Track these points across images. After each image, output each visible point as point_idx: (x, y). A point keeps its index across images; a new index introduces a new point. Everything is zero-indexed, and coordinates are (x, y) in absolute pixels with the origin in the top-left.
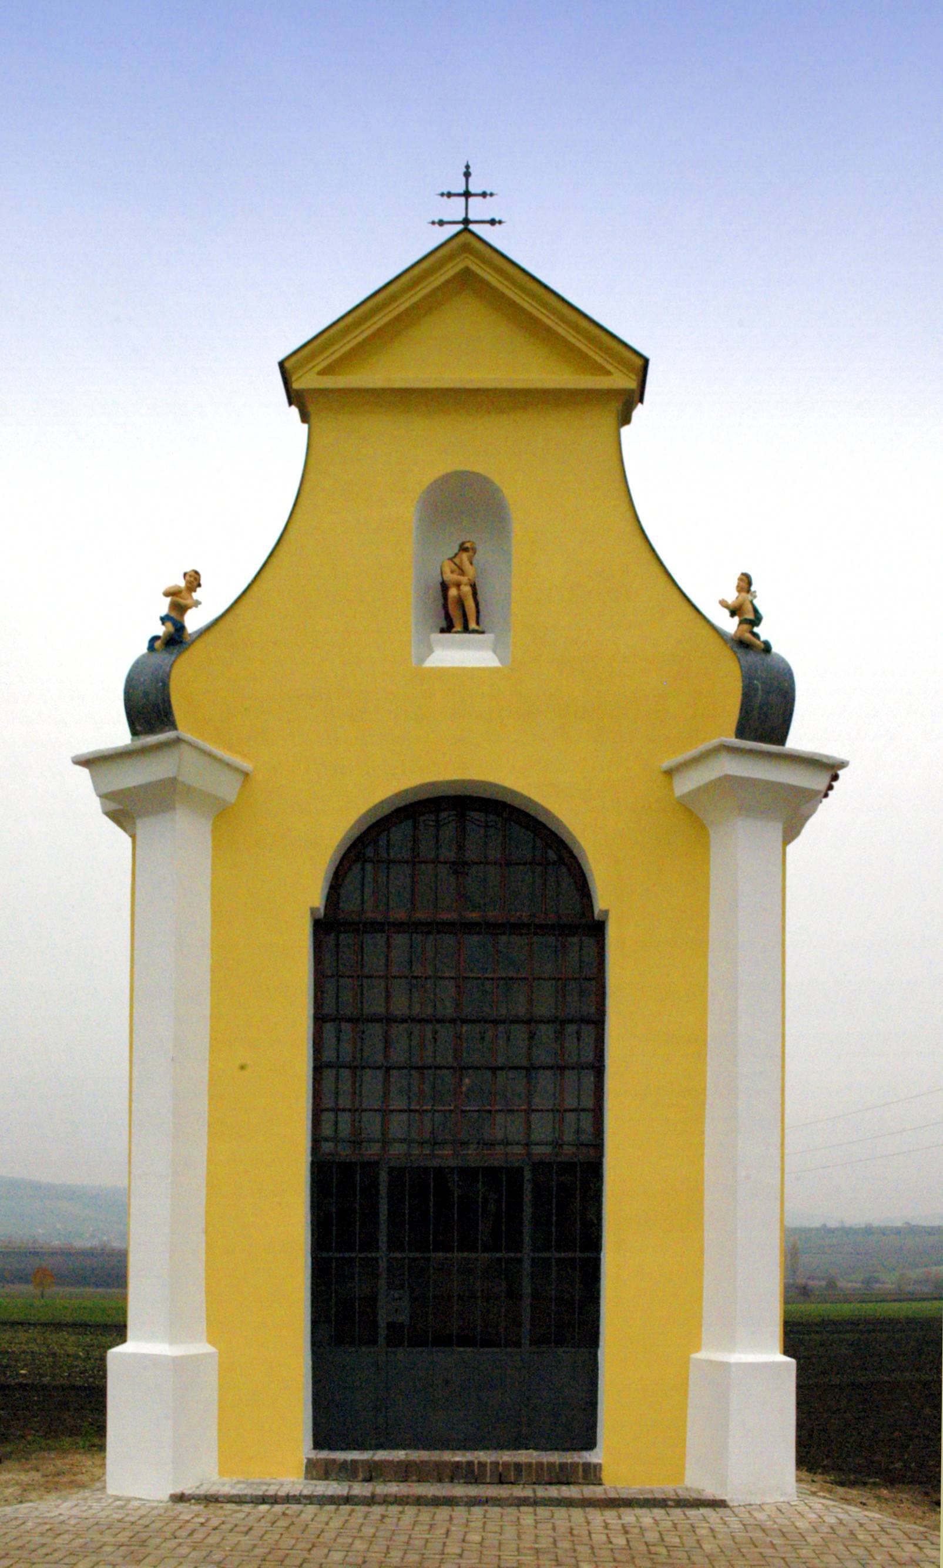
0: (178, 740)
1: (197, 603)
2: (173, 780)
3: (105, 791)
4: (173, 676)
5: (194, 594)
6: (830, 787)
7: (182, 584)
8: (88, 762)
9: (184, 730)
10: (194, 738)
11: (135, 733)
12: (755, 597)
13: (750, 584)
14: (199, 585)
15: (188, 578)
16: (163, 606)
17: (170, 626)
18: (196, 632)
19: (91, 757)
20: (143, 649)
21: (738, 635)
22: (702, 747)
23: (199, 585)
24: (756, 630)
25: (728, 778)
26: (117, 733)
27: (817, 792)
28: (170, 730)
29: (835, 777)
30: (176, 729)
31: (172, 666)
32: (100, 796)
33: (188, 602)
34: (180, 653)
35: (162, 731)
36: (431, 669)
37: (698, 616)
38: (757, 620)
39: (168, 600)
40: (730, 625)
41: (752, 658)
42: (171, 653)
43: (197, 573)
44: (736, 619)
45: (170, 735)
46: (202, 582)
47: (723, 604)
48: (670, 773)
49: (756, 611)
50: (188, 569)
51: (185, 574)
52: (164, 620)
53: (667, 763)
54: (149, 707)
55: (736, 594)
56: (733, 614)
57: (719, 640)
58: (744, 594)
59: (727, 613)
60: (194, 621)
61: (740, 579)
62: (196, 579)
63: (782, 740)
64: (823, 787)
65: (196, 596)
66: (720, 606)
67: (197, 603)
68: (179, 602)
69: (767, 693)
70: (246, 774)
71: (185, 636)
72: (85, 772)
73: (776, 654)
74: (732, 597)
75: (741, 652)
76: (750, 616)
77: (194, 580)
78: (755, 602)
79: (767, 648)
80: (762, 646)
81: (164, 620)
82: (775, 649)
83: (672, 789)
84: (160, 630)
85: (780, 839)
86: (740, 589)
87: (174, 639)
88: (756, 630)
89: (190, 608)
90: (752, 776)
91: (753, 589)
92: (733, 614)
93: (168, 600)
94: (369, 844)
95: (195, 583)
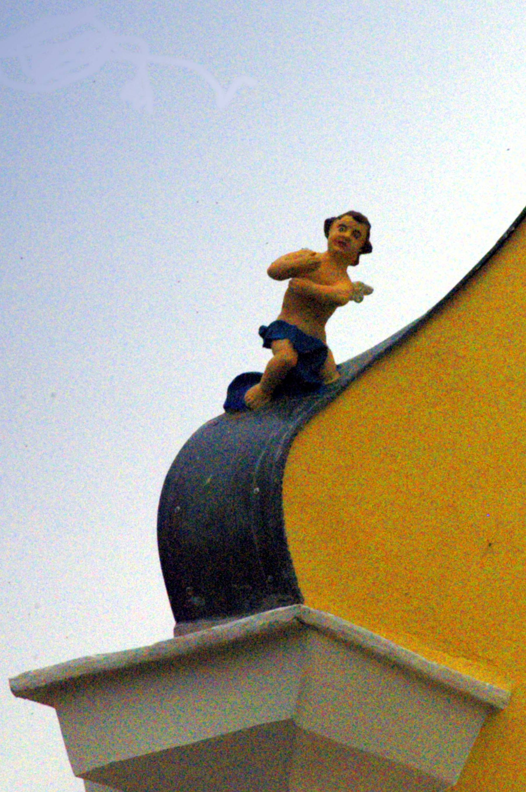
0: (302, 628)
1: (360, 292)
2: (290, 723)
3: (88, 768)
4: (293, 469)
5: (351, 270)
7: (320, 245)
8: (63, 690)
9: (319, 603)
10: (347, 623)
11: (183, 612)
14: (367, 248)
15: (334, 232)
16: (271, 301)
17: (285, 349)
18: (355, 360)
19: (61, 676)
20: (215, 407)
23: (367, 248)
26: (140, 615)
28: (283, 603)
30: (296, 597)
31: (288, 445)
32: (85, 776)
33: (339, 287)
34: (312, 414)
35: (254, 608)
39: (284, 285)
42: (288, 417)
43: (359, 218)
45: (281, 614)
46: (373, 240)
50: (336, 211)
51: (328, 224)
52: (268, 335)
54: (223, 543)
60: (348, 336)
62: (356, 234)
65: (355, 274)
67: (360, 292)
68: (312, 290)
70: (491, 710)
71: (327, 370)
72: (48, 714)
77: (352, 237)
81: (268, 335)
84: (259, 359)
87: (298, 378)
89: (341, 303)
93: (284, 285)
94: (386, 700)
95: (355, 244)
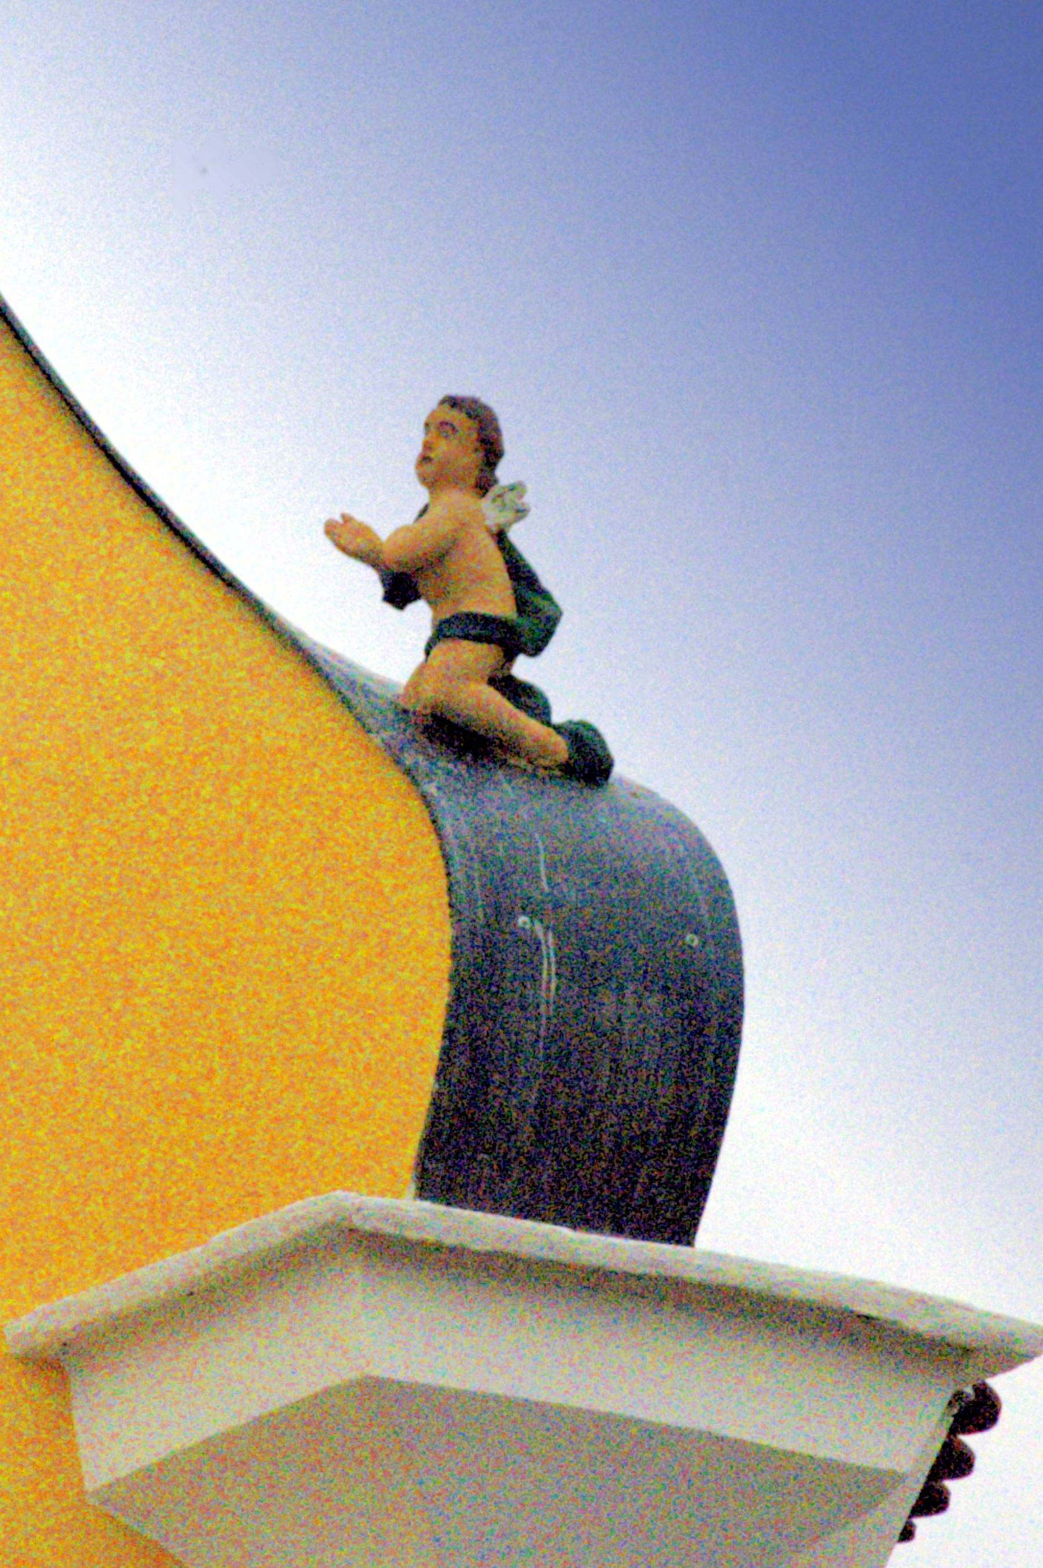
6: (954, 1462)
12: (521, 513)
13: (491, 451)
21: (429, 693)
22: (234, 1238)
24: (523, 668)
25: (382, 1400)
27: (881, 1483)
29: (978, 1411)
36: (960, 1443)
37: (217, 591)
38: (525, 622)
40: (390, 647)
41: (514, 806)
44: (420, 616)
47: (348, 538)
48: (54, 1365)
49: (521, 575)
53: (35, 1321)
55: (421, 496)
56: (400, 590)
57: (324, 712)
58: (459, 501)
59: (370, 584)
61: (438, 427)
63: (681, 1228)
64: (912, 1453)
66: (327, 544)
69: (585, 971)
73: (621, 780)
74: (395, 508)
75: (442, 772)
76: (497, 601)
78: (517, 535)
79: (587, 762)
80: (561, 748)
82: (628, 766)
83: (66, 1460)
85: (912, 1501)
86: (433, 472)
88: (523, 668)
90: (604, 1405)
91: (505, 473)
92: (400, 590)
